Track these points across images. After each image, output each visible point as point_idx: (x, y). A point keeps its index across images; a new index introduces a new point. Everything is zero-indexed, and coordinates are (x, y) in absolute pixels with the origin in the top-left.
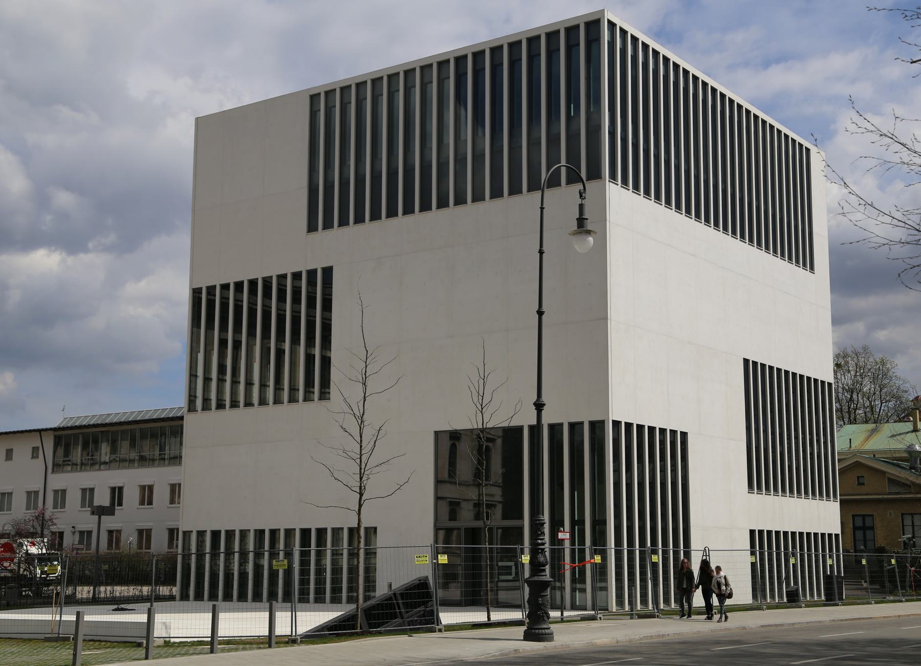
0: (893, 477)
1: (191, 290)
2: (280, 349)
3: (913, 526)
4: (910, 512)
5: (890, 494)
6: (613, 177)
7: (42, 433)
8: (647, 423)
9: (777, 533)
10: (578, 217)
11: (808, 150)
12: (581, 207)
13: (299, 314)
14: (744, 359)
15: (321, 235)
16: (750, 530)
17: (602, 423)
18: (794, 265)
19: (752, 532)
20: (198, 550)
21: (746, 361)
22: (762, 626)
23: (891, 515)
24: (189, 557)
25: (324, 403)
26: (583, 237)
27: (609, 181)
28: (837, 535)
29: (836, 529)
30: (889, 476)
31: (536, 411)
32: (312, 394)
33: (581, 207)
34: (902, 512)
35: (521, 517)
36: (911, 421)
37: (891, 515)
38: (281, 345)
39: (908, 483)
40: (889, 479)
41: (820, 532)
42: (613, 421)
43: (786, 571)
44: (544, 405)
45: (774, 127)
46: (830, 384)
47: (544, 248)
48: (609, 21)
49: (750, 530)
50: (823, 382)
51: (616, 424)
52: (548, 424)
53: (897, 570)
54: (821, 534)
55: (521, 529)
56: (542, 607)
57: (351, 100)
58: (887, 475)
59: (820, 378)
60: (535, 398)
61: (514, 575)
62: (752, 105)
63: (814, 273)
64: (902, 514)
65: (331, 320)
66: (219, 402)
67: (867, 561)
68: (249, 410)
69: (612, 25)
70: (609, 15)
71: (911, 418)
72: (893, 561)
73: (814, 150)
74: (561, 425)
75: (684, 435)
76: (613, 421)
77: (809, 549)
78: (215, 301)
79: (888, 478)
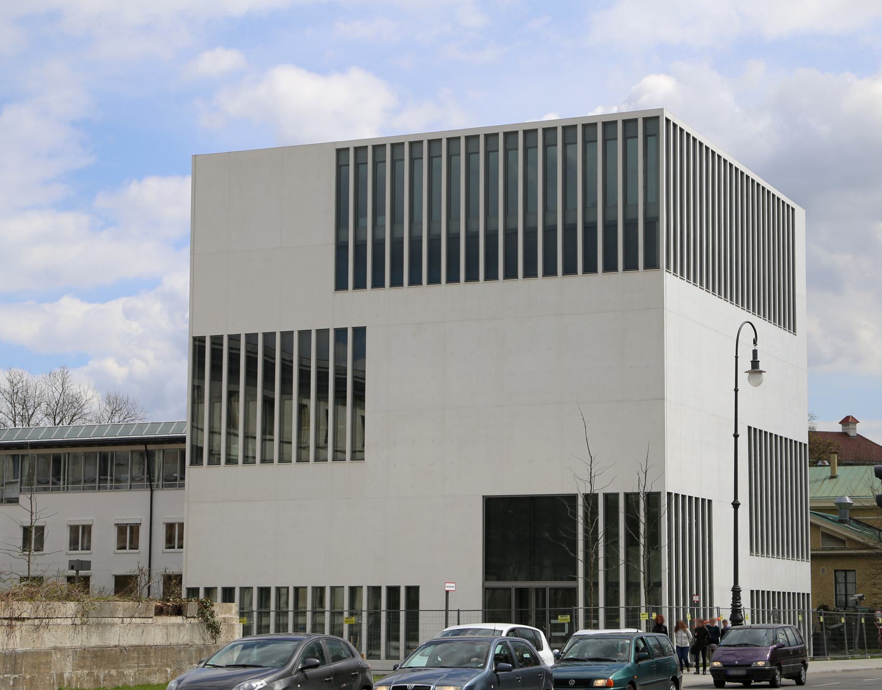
0: (829, 532)
1: (191, 338)
2: (301, 404)
3: (846, 583)
4: (843, 569)
5: (824, 549)
6: (668, 267)
7: (848, 573)
8: (687, 494)
9: (763, 592)
10: (752, 360)
11: (793, 209)
12: (755, 352)
13: (291, 364)
14: (748, 426)
15: (351, 295)
16: (751, 590)
17: (658, 495)
18: (729, 302)
19: (752, 592)
20: (276, 607)
21: (749, 428)
22: (844, 671)
23: (823, 571)
24: (173, 614)
25: (357, 464)
26: (758, 375)
27: (666, 271)
28: (808, 594)
29: (807, 589)
30: (823, 531)
31: (733, 509)
32: (199, 432)
33: (755, 352)
34: (836, 568)
35: (575, 579)
36: (827, 466)
37: (823, 571)
38: (302, 401)
39: (843, 538)
40: (823, 533)
41: (761, 589)
42: (668, 492)
43: (814, 629)
44: (740, 504)
45: (755, 181)
46: (805, 445)
47: (739, 387)
48: (666, 119)
49: (751, 590)
50: (800, 443)
51: (669, 494)
52: (604, 493)
53: (845, 627)
54: (756, 591)
55: (574, 591)
56: (74, 688)
57: (385, 158)
58: (822, 530)
59: (799, 440)
60: (733, 500)
61: (567, 631)
62: (756, 174)
63: (796, 335)
64: (835, 571)
65: (364, 379)
66: (228, 457)
67: (865, 621)
68: (267, 467)
69: (668, 121)
70: (667, 114)
71: (826, 461)
72: (843, 620)
73: (800, 215)
74: (617, 495)
75: (710, 501)
76: (668, 492)
77: (678, 603)
78: (222, 351)
79: (822, 532)
